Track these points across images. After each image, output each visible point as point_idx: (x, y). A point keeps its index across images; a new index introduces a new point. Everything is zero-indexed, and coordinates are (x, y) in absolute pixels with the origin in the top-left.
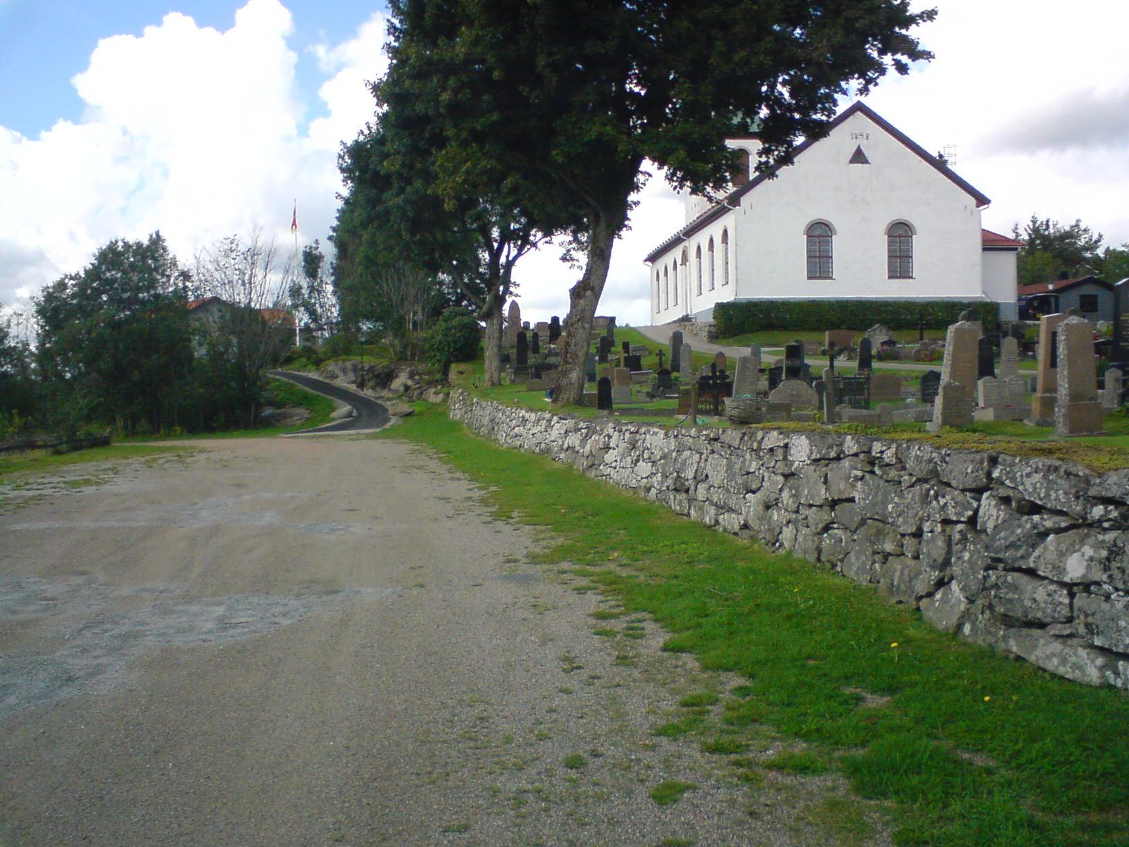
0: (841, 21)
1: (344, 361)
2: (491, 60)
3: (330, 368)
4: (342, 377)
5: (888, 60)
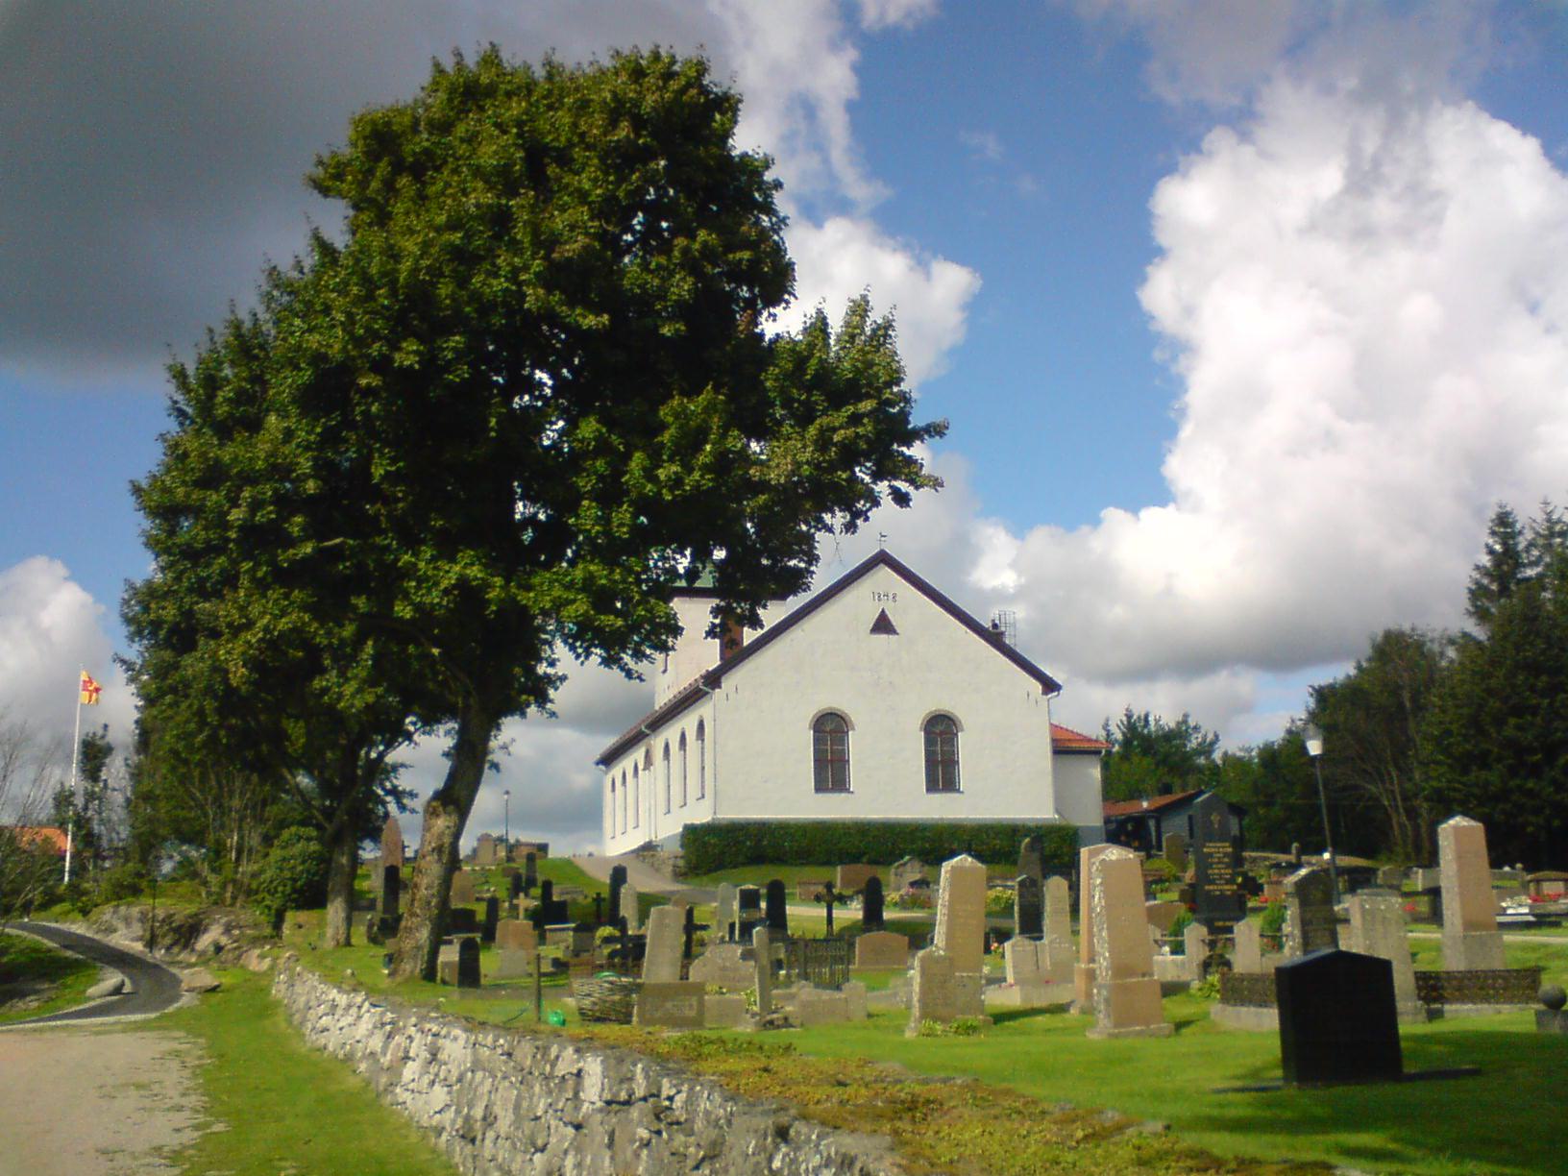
0: (812, 431)
1: (129, 905)
2: (305, 464)
3: (107, 917)
4: (122, 930)
5: (882, 488)
